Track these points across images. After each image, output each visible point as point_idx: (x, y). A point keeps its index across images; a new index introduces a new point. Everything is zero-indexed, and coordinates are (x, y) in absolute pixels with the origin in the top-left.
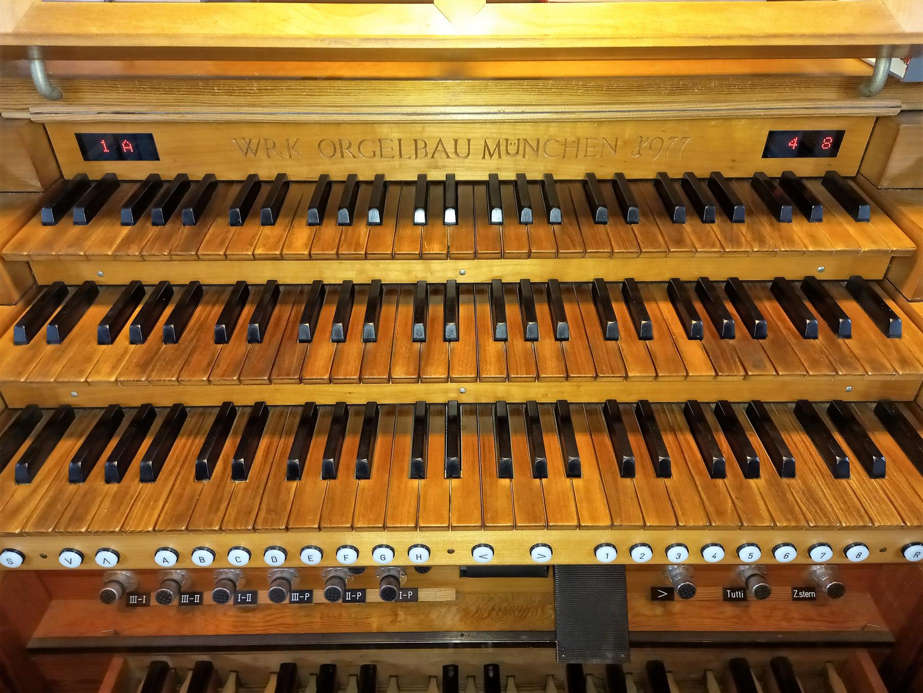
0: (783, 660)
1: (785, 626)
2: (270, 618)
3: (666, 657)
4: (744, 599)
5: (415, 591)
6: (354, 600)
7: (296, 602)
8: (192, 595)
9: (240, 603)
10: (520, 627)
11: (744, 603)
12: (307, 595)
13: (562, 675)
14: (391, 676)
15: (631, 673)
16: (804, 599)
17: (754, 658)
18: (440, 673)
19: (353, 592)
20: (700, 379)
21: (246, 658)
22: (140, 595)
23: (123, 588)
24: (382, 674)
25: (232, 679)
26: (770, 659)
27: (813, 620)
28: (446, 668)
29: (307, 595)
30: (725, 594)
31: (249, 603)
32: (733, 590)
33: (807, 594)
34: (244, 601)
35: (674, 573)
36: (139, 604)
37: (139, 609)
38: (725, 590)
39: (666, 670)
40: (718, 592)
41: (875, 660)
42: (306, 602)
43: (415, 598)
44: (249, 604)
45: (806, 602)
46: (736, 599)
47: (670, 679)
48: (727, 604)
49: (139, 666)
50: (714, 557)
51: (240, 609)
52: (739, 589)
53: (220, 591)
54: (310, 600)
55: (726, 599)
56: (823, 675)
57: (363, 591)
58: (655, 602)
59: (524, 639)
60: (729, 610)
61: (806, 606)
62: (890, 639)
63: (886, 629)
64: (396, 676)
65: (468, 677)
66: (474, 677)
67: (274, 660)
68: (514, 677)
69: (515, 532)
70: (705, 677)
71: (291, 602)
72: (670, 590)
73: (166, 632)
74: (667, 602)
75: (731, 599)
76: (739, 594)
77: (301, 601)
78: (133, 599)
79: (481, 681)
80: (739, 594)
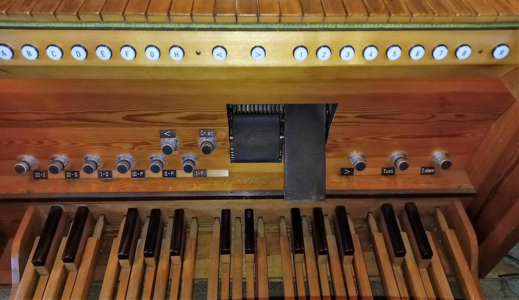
0: (412, 204)
1: (415, 187)
2: (120, 185)
3: (349, 204)
4: (393, 174)
5: (205, 171)
6: (169, 176)
7: (135, 177)
8: (73, 172)
9: (101, 177)
10: (265, 188)
11: (393, 176)
12: (141, 173)
13: (288, 216)
14: (193, 218)
15: (327, 215)
16: (428, 173)
17: (398, 205)
18: (219, 215)
19: (169, 171)
20: (381, 117)
21: (107, 206)
22: (41, 172)
23: (29, 167)
24: (188, 216)
25: (101, 219)
26: (404, 205)
27: (431, 183)
28: (246, 211)
29: (141, 173)
30: (383, 171)
31: (107, 177)
32: (387, 169)
33: (429, 171)
34: (104, 176)
35: (354, 158)
36: (41, 178)
37: (42, 180)
38: (383, 169)
39: (347, 213)
40: (379, 171)
41: (464, 205)
42: (141, 177)
43: (205, 175)
44: (106, 176)
45: (429, 175)
46: (389, 174)
47: (349, 217)
48: (384, 176)
49: (44, 210)
50: (371, 55)
51: (102, 180)
52: (391, 169)
53: (87, 166)
54: (143, 176)
55: (383, 174)
56: (434, 215)
57: (175, 171)
58: (343, 176)
59: (267, 194)
60: (384, 179)
61: (429, 177)
62: (474, 191)
63: (472, 187)
64: (196, 218)
65: (237, 218)
66: (240, 218)
67: (124, 207)
68: (262, 218)
69: (309, 283)
70: (368, 216)
71: (132, 177)
72: (352, 170)
73: (57, 191)
74: (350, 176)
75: (386, 174)
76: (391, 171)
77: (138, 176)
78: (38, 175)
79: (243, 220)
80: (391, 171)
